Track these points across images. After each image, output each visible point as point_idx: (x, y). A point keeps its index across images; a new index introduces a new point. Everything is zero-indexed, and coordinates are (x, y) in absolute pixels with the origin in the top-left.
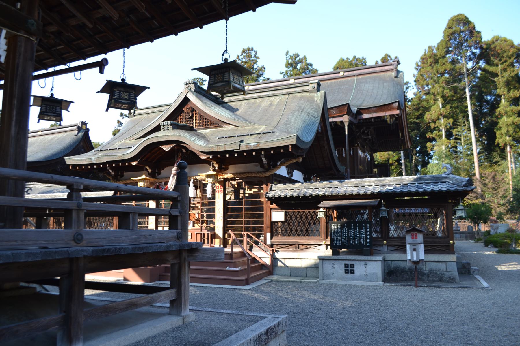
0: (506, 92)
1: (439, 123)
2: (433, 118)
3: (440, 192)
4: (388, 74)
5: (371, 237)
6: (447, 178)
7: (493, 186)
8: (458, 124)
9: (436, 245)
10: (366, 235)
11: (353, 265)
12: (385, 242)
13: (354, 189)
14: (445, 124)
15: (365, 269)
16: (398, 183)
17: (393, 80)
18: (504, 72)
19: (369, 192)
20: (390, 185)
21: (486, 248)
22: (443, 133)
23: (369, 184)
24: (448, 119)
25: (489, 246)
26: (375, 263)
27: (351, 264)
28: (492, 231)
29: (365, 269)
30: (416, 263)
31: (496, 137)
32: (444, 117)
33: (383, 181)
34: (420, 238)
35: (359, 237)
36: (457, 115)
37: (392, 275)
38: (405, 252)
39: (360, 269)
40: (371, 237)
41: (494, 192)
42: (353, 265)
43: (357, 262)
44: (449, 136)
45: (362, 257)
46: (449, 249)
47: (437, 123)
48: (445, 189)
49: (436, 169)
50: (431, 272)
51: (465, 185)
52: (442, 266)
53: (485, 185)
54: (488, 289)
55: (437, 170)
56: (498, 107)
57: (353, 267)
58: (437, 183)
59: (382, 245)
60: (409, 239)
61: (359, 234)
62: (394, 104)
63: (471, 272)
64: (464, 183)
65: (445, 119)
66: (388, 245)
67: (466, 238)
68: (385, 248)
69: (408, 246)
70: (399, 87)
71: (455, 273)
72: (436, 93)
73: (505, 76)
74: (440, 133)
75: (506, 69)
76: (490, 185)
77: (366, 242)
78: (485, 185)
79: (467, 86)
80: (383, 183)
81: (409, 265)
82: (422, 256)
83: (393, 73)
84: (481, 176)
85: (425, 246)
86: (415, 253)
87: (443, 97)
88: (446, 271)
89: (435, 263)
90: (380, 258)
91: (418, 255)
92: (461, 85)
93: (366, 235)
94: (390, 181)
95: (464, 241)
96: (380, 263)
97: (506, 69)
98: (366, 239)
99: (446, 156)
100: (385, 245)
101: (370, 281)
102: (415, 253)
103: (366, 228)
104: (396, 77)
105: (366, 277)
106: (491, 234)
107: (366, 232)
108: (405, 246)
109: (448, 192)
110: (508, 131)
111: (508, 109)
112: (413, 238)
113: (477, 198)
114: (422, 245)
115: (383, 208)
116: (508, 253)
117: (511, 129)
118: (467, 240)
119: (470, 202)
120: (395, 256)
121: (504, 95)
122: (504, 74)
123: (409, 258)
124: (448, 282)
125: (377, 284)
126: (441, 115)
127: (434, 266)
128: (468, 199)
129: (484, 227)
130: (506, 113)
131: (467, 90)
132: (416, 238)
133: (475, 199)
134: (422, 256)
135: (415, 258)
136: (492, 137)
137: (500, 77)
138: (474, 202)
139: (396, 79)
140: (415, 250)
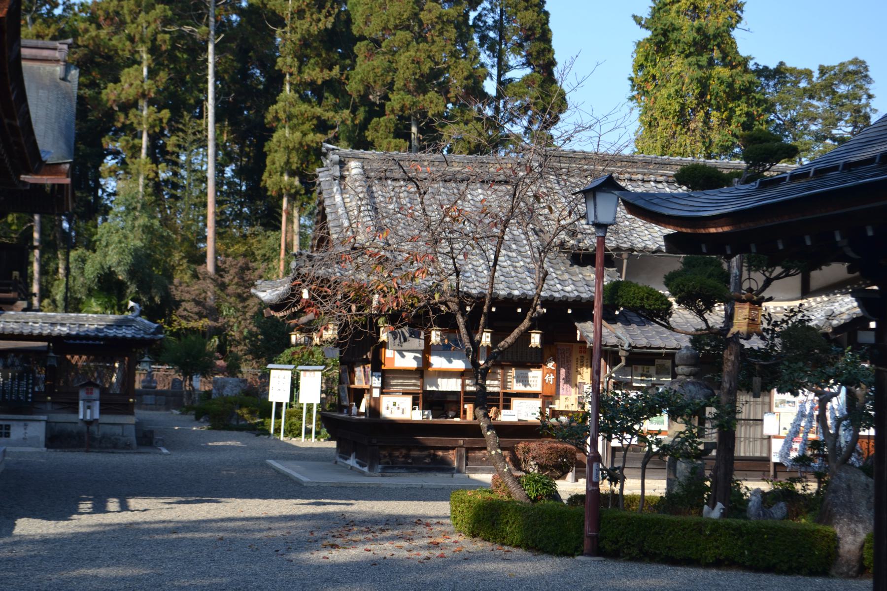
0: (294, 70)
1: (136, 116)
2: (123, 97)
3: (124, 338)
4: (48, 67)
5: (33, 392)
6: (133, 321)
7: (239, 291)
8: (181, 126)
9: (116, 403)
10: (28, 388)
11: (9, 426)
12: (49, 398)
13: (15, 326)
14: (150, 120)
15: (23, 432)
16: (72, 321)
17: (57, 86)
18: (299, 18)
19: (36, 332)
20: (62, 325)
21: (197, 422)
22: (145, 141)
23: (35, 320)
24: (159, 110)
25: (202, 420)
26: (38, 424)
27: (6, 426)
28: (214, 391)
29: (23, 432)
30: (89, 423)
31: (265, 166)
32: (151, 102)
33: (54, 317)
34: (96, 393)
35: (18, 390)
36: (179, 101)
37: (56, 439)
38: (76, 412)
39: (17, 432)
40: (33, 392)
41: (240, 306)
42: (9, 426)
43: (14, 423)
44: (157, 153)
45: (22, 417)
46: (128, 410)
47: (131, 116)
48: (129, 336)
49: (116, 239)
50: (104, 436)
51: (153, 333)
52: (118, 430)
53: (223, 287)
54: (166, 454)
55: (120, 242)
56: (275, 102)
57: (9, 429)
58: (120, 326)
59: (46, 402)
60: (82, 394)
61: (18, 387)
62: (63, 166)
63: (154, 442)
64: (152, 330)
65: (153, 109)
66: (53, 402)
67: (168, 407)
68: (49, 407)
69: (81, 403)
70: (68, 103)
71: (133, 439)
72: (137, 37)
73: (299, 30)
74: (136, 141)
75: (304, 11)
76: (231, 289)
77: (27, 398)
78: (223, 287)
79: (211, 37)
80: (54, 321)
81: (80, 425)
82: (97, 416)
83: (58, 69)
84: (218, 269)
85: (101, 405)
86: (88, 411)
87: (154, 50)
88: (123, 436)
89: (110, 426)
90: (44, 417)
91: (92, 414)
92: (199, 32)
93: (28, 388)
94: (63, 319)
95: (163, 412)
96: (43, 424)
97: (304, 11)
98: (27, 393)
99: (144, 206)
100: (49, 401)
101: (30, 446)
102: (88, 411)
103: (28, 379)
104: (64, 79)
105: (24, 441)
106: (213, 396)
107: (28, 384)
108: (78, 404)
109: (133, 339)
110: (288, 162)
111: (295, 111)
112: (87, 393)
113: (201, 316)
114: (98, 403)
115: (52, 354)
116: (224, 429)
117: (295, 160)
118: (168, 409)
119: (184, 324)
120: (62, 417)
121: (291, 74)
122: (298, 23)
123: (81, 417)
124: (123, 448)
125: (38, 450)
126: (144, 95)
127: (107, 429)
128: (182, 317)
129: (200, 384)
130: (290, 118)
131: (211, 47)
132: (92, 393)
133: (197, 317)
134: (97, 416)
135: (88, 417)
136: (253, 169)
137: (288, 29)
138: (192, 324)
139: (62, 83)
140: (89, 407)
